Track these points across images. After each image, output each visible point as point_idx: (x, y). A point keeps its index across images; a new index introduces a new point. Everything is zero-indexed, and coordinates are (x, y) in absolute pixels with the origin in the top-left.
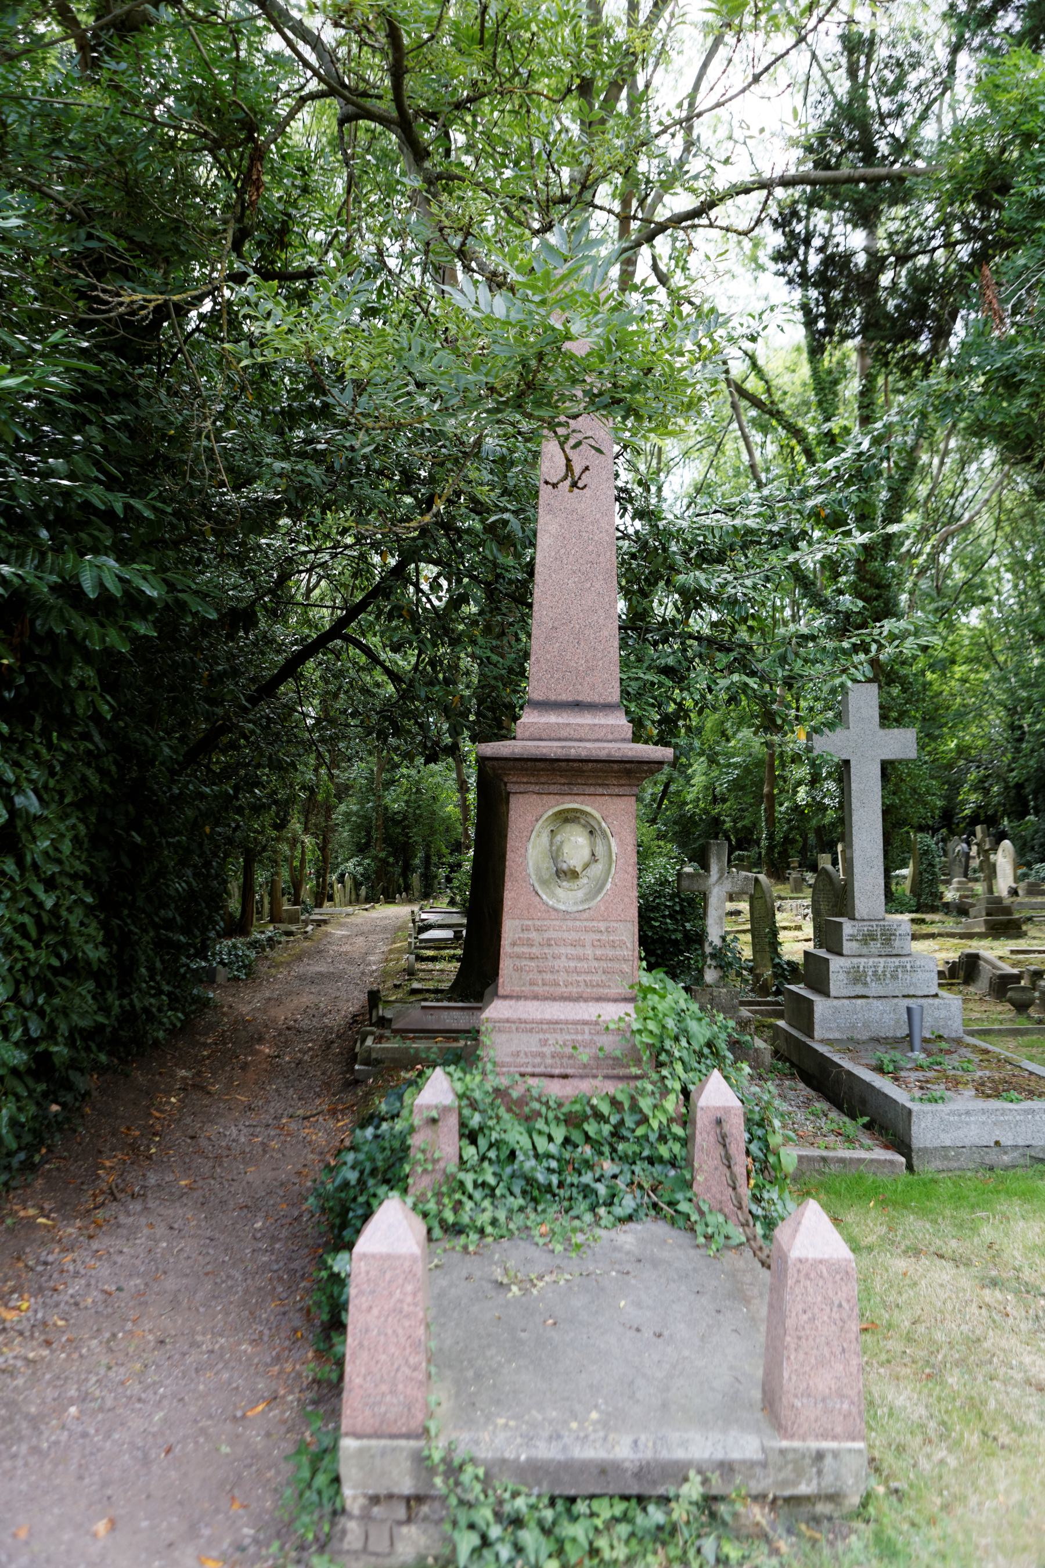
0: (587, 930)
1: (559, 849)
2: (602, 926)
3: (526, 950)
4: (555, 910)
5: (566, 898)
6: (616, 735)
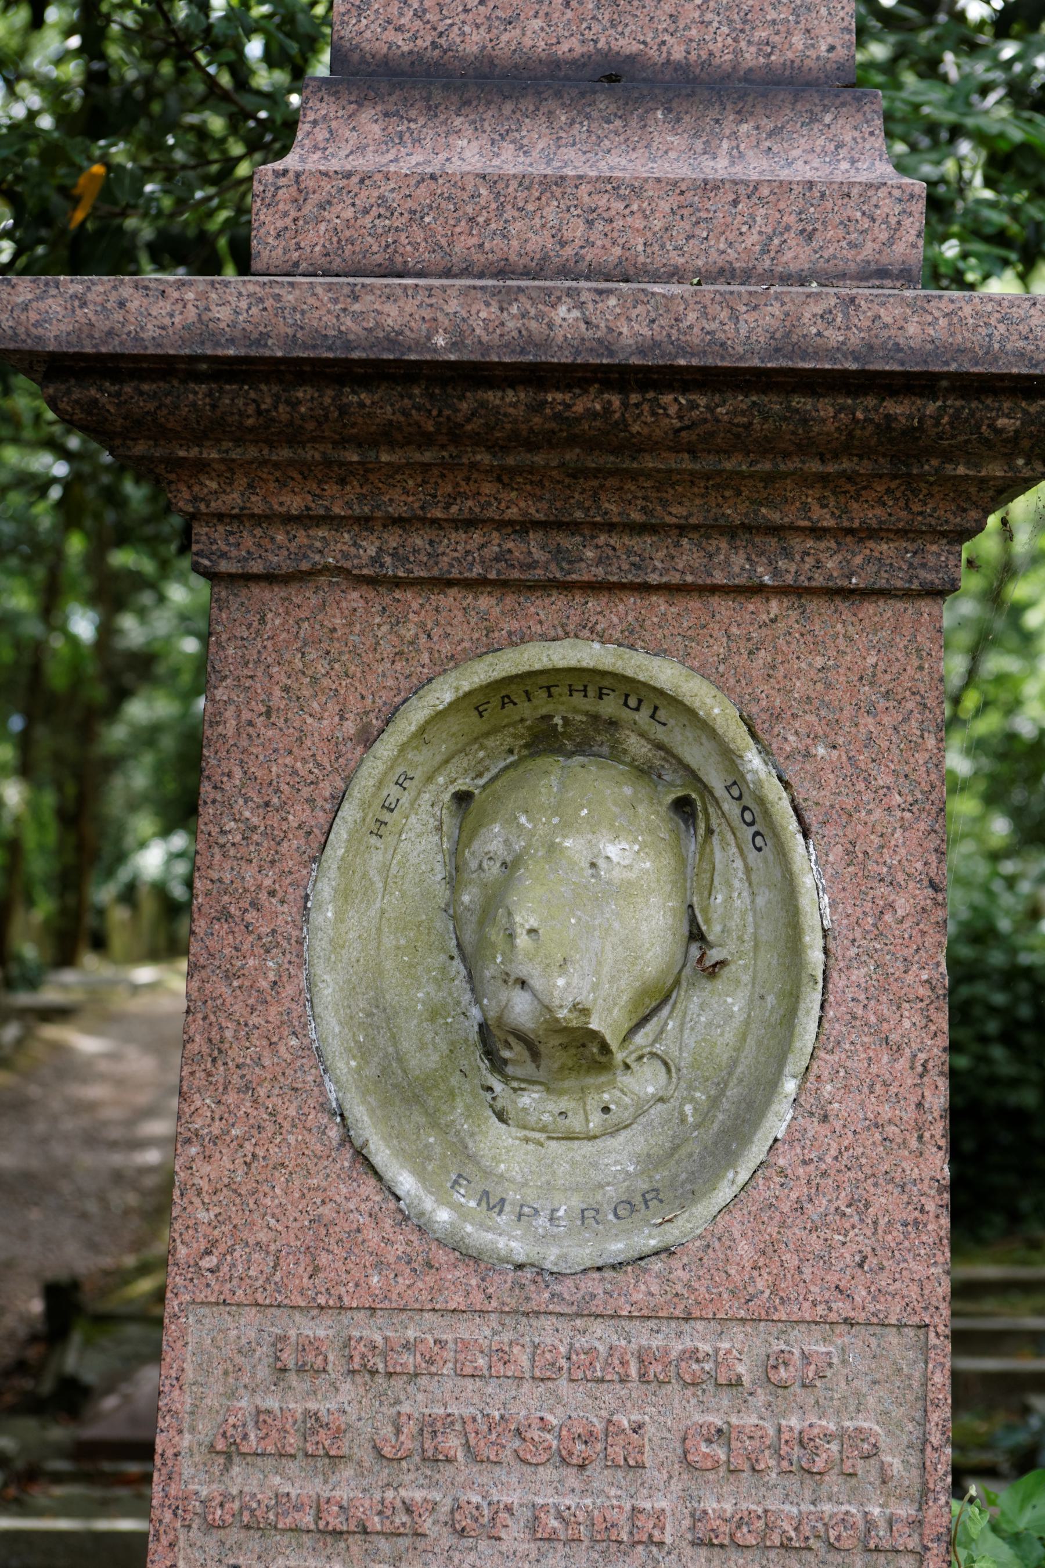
0: (650, 1372)
1: (494, 904)
2: (742, 1351)
3: (298, 1484)
4: (471, 1257)
5: (538, 1182)
6: (833, 246)
